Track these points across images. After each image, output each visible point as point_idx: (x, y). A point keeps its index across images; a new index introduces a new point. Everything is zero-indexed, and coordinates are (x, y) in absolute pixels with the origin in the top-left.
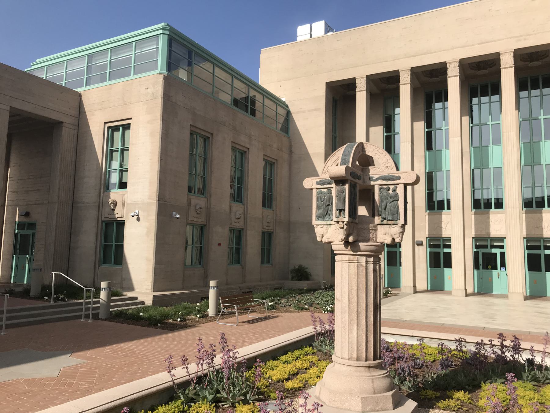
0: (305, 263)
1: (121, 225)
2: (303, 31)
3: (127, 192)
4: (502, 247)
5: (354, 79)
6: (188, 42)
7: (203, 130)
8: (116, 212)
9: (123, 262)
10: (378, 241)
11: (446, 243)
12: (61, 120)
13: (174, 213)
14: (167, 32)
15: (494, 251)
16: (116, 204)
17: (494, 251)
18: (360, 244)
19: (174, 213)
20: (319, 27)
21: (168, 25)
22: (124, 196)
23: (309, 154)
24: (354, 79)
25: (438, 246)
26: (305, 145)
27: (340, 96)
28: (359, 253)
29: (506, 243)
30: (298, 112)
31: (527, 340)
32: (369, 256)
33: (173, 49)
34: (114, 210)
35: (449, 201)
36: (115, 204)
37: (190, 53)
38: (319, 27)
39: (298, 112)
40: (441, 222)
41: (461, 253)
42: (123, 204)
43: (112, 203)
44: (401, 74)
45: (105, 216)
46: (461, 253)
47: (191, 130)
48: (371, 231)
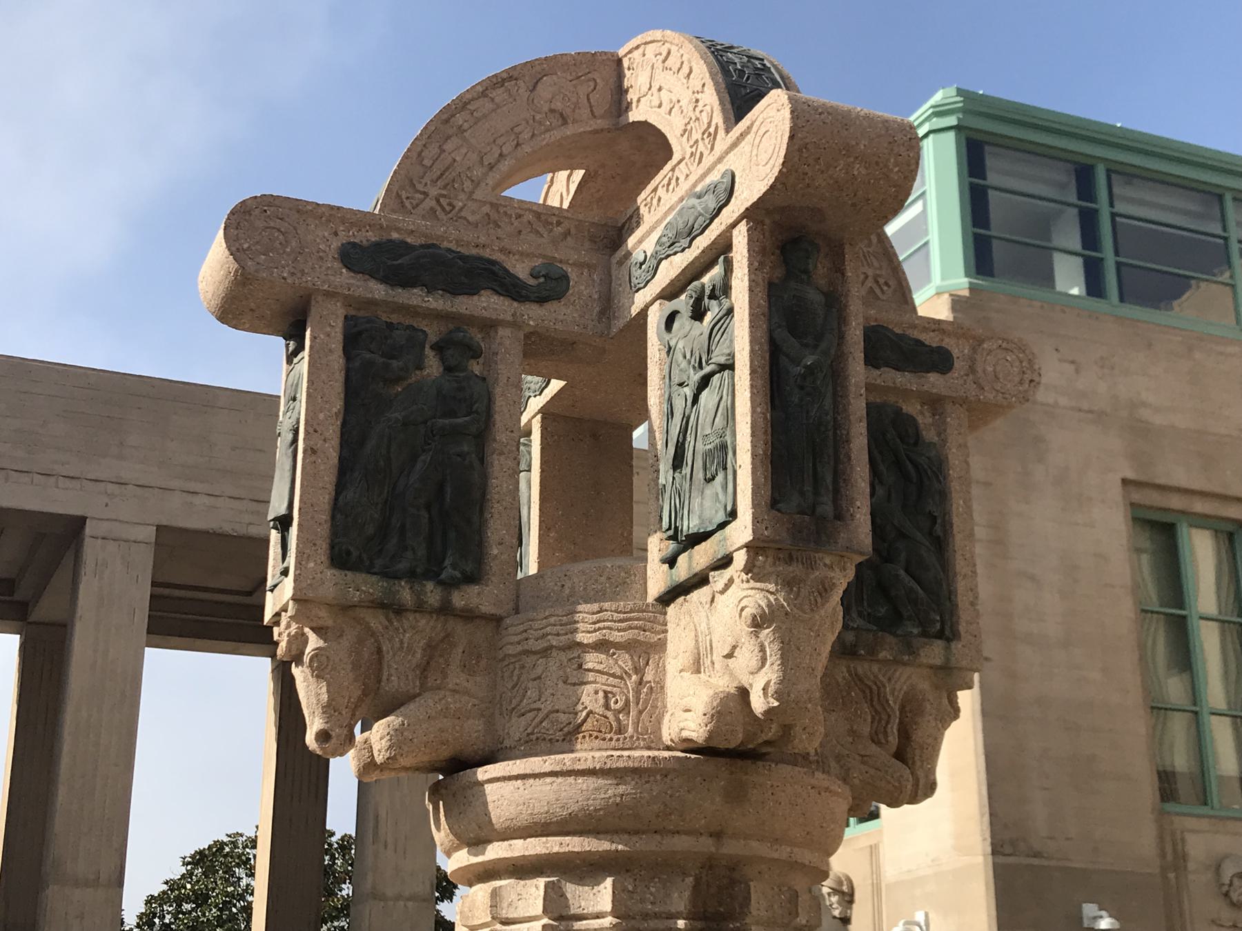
3: (880, 832)
6: (1147, 153)
7: (1203, 494)
10: (668, 733)
13: (1089, 909)
14: (952, 121)
16: (852, 895)
18: (483, 773)
19: (1089, 909)
21: (960, 92)
22: (873, 850)
28: (496, 851)
32: (585, 869)
33: (993, 178)
36: (848, 898)
37: (1084, 176)
42: (877, 889)
43: (835, 891)
47: (1133, 505)
48: (592, 660)
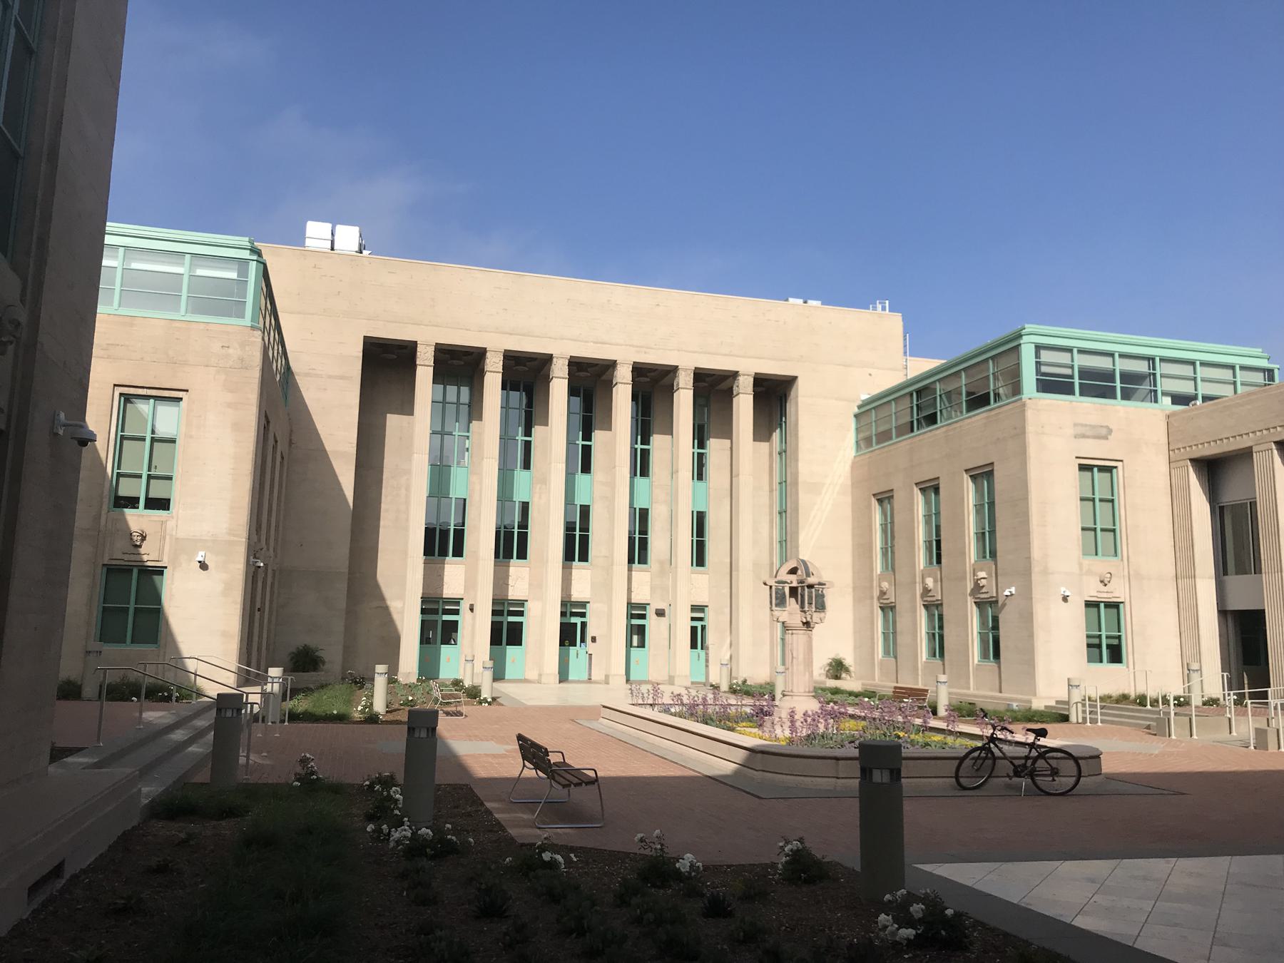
0: (311, 641)
1: (152, 574)
2: (317, 232)
4: (583, 615)
5: (415, 344)
8: (142, 550)
9: (162, 635)
11: (518, 608)
12: (829, 601)
15: (574, 620)
17: (574, 620)
20: (348, 237)
23: (325, 451)
24: (415, 344)
25: (435, 612)
26: (318, 434)
27: (386, 364)
29: (589, 610)
30: (307, 375)
31: (489, 801)
34: (140, 546)
35: (459, 535)
38: (348, 237)
39: (307, 375)
40: (507, 576)
41: (542, 624)
44: (488, 354)
45: (117, 553)
46: (542, 624)
